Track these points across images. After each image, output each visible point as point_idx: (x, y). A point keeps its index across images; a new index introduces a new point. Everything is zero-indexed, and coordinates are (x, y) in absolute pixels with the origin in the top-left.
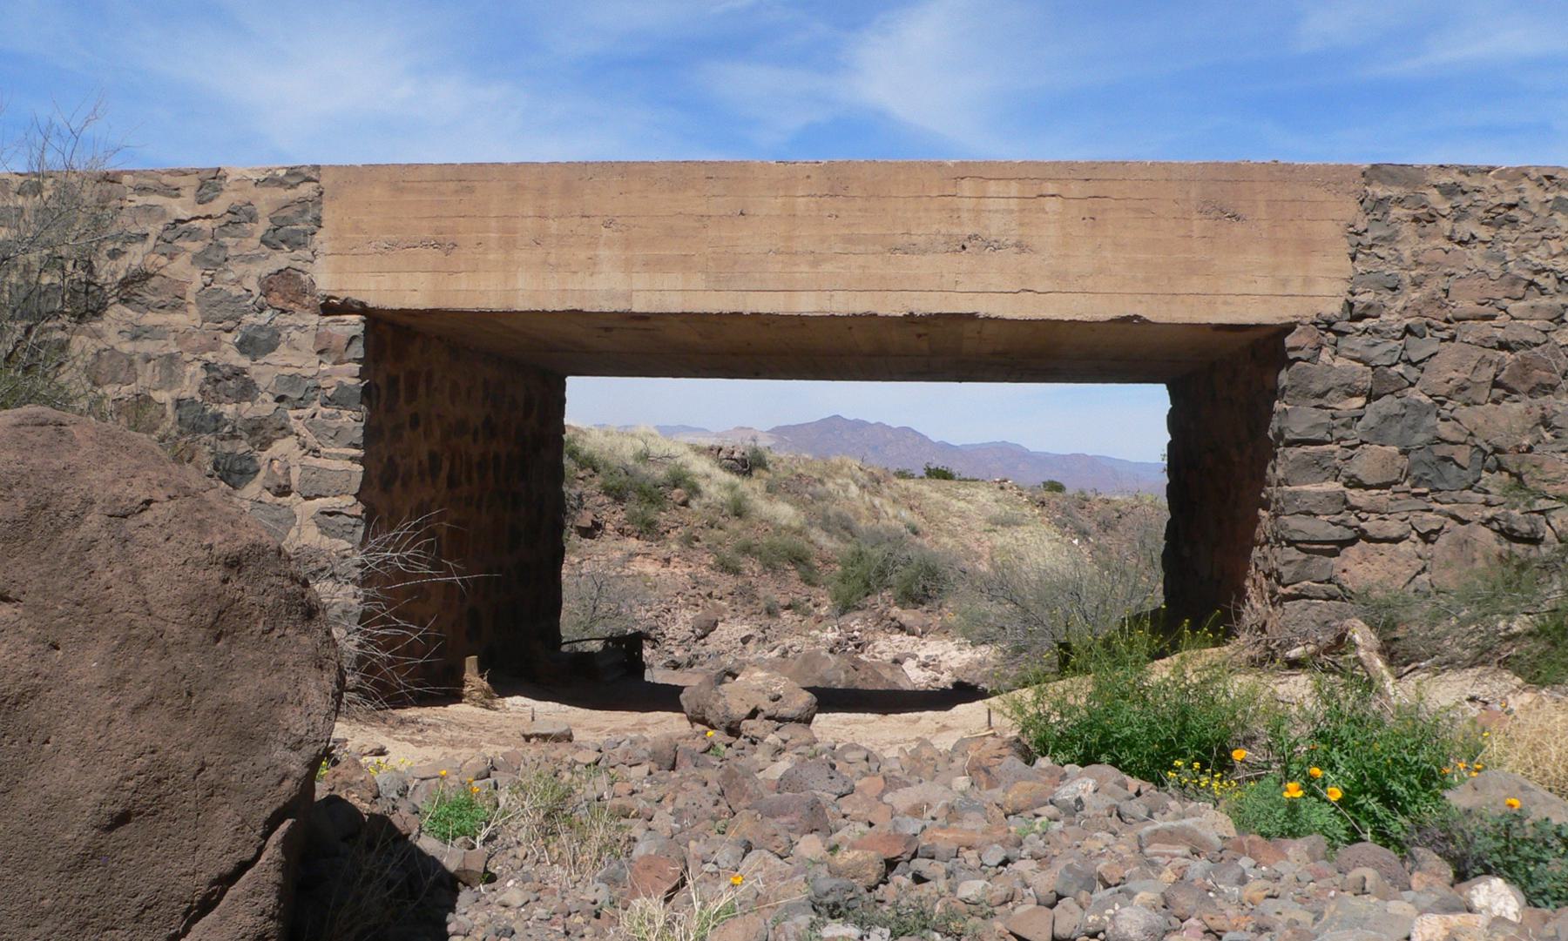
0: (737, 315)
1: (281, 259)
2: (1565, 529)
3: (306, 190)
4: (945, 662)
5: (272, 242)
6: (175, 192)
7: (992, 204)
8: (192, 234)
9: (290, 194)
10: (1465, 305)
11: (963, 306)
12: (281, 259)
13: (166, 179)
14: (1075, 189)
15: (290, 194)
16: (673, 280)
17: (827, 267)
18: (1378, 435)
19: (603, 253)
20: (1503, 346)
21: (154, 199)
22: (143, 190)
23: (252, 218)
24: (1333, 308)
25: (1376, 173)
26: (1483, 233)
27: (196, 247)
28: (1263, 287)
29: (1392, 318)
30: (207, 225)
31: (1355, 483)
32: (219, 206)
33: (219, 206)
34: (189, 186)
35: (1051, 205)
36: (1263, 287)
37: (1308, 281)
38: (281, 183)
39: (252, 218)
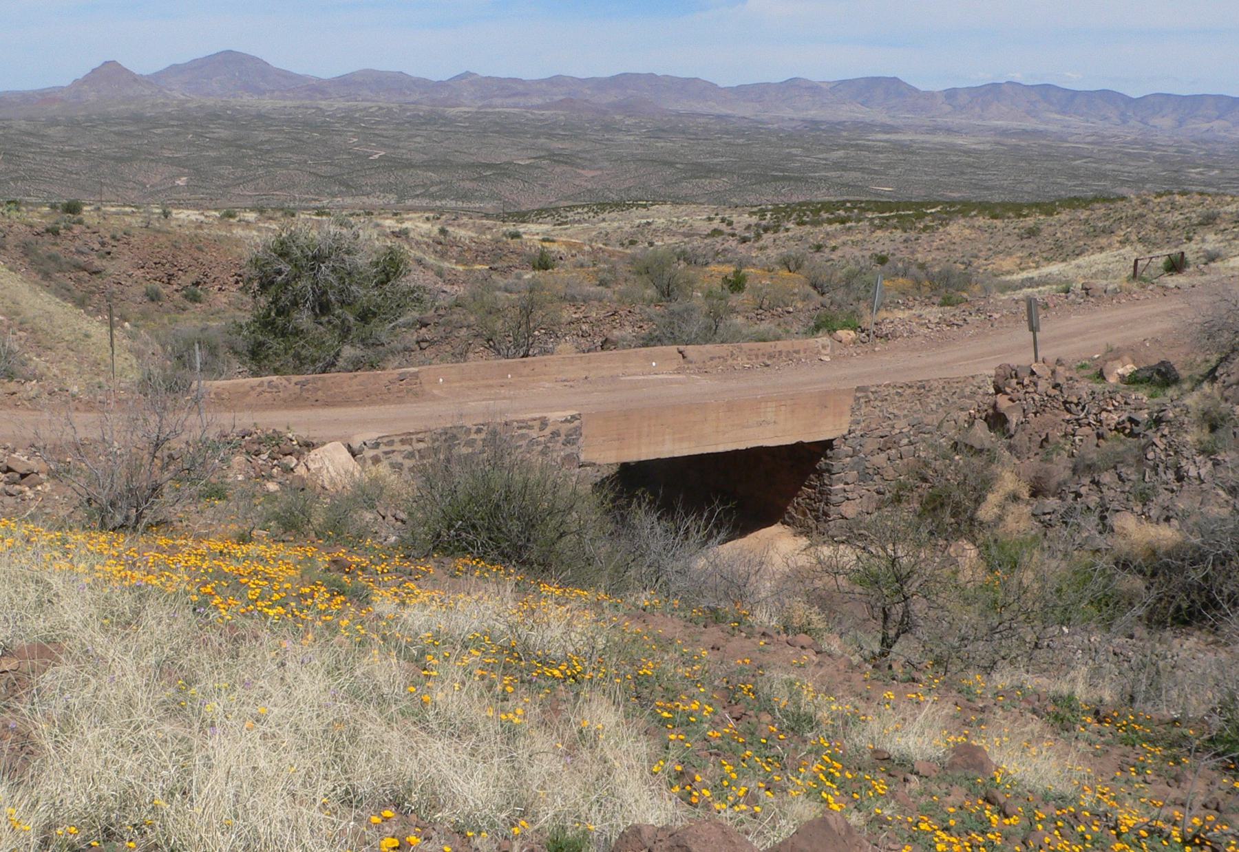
0: (737, 451)
1: (569, 450)
2: (1237, 590)
3: (577, 423)
4: (750, 717)
5: (567, 442)
6: (530, 427)
7: (769, 409)
8: (538, 444)
9: (572, 425)
10: (873, 426)
11: (760, 444)
12: (569, 450)
13: (529, 423)
14: (789, 402)
15: (572, 425)
16: (685, 445)
17: (727, 435)
18: (852, 469)
19: (667, 437)
20: (882, 437)
21: (524, 431)
22: (520, 428)
23: (559, 435)
24: (846, 432)
25: (859, 389)
26: (880, 404)
27: (540, 448)
28: (831, 427)
29: (858, 433)
30: (543, 439)
31: (847, 484)
32: (547, 431)
33: (547, 431)
34: (537, 424)
35: (783, 408)
36: (831, 427)
37: (841, 424)
38: (569, 421)
39: (559, 435)
